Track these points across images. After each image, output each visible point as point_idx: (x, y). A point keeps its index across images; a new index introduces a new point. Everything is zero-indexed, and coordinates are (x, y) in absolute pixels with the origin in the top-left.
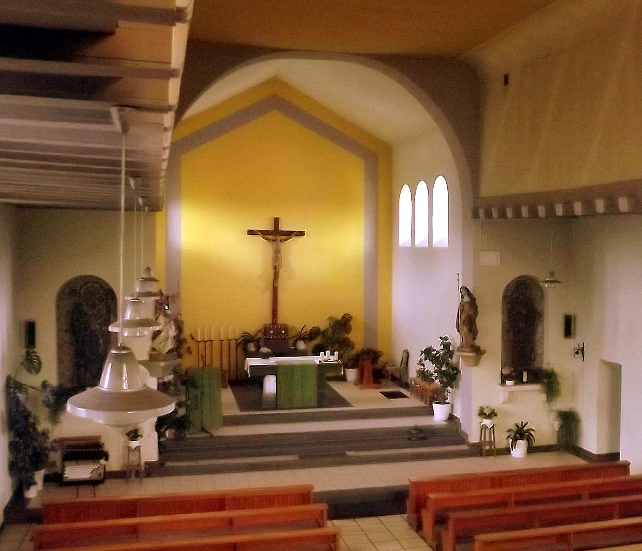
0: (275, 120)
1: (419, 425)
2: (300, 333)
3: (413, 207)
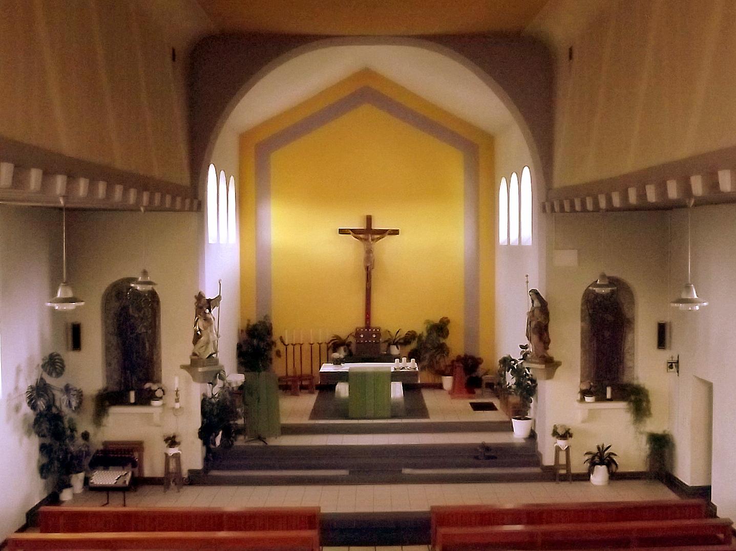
0: (366, 111)
1: (486, 442)
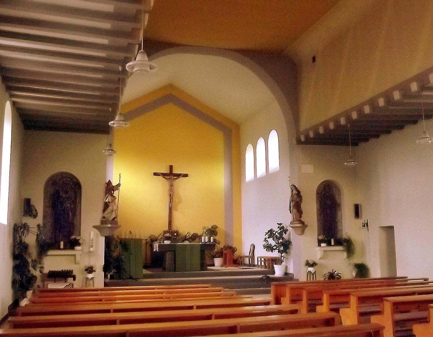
0: (170, 108)
2: (186, 236)
3: (255, 160)
